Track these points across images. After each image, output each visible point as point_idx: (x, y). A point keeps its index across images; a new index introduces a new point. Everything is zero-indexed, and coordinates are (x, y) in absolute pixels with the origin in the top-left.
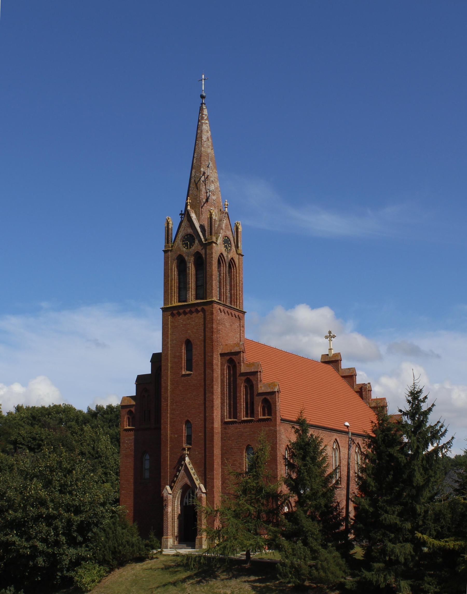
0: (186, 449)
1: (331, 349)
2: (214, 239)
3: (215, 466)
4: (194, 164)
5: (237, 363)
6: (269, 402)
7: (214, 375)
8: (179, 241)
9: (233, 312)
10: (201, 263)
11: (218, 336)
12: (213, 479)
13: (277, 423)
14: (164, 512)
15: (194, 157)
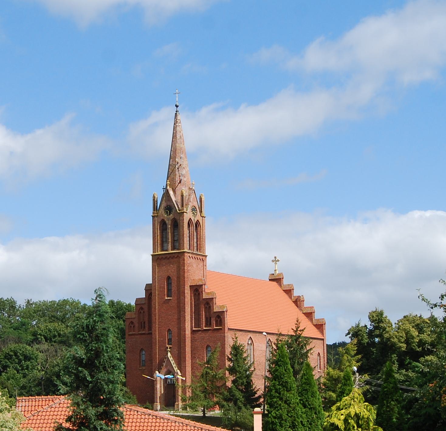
0: (169, 347)
1: (275, 270)
2: (185, 211)
3: (187, 358)
4: (171, 155)
5: (200, 292)
6: (220, 317)
7: (186, 300)
9: (198, 257)
10: (176, 225)
11: (188, 274)
12: (186, 367)
13: (226, 331)
14: (155, 388)
15: (171, 150)
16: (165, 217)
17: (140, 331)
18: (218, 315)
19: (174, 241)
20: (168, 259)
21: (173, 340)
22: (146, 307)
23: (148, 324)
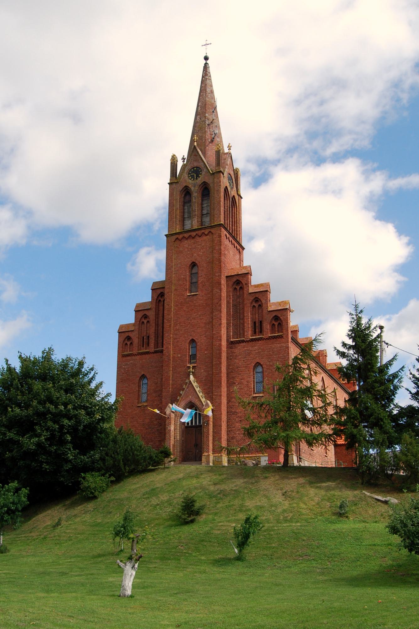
8: (186, 175)
12: (221, 396)
14: (167, 430)
16: (189, 183)
17: (141, 350)
18: (275, 316)
19: (202, 215)
20: (193, 238)
21: (198, 355)
22: (151, 315)
23: (154, 339)
